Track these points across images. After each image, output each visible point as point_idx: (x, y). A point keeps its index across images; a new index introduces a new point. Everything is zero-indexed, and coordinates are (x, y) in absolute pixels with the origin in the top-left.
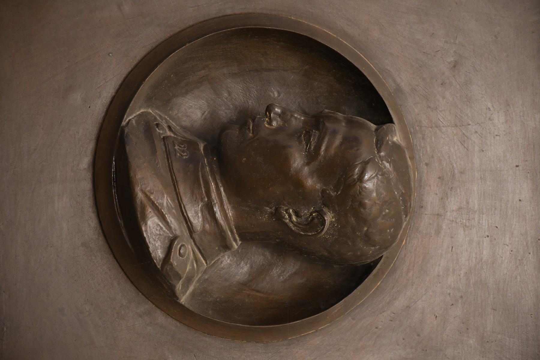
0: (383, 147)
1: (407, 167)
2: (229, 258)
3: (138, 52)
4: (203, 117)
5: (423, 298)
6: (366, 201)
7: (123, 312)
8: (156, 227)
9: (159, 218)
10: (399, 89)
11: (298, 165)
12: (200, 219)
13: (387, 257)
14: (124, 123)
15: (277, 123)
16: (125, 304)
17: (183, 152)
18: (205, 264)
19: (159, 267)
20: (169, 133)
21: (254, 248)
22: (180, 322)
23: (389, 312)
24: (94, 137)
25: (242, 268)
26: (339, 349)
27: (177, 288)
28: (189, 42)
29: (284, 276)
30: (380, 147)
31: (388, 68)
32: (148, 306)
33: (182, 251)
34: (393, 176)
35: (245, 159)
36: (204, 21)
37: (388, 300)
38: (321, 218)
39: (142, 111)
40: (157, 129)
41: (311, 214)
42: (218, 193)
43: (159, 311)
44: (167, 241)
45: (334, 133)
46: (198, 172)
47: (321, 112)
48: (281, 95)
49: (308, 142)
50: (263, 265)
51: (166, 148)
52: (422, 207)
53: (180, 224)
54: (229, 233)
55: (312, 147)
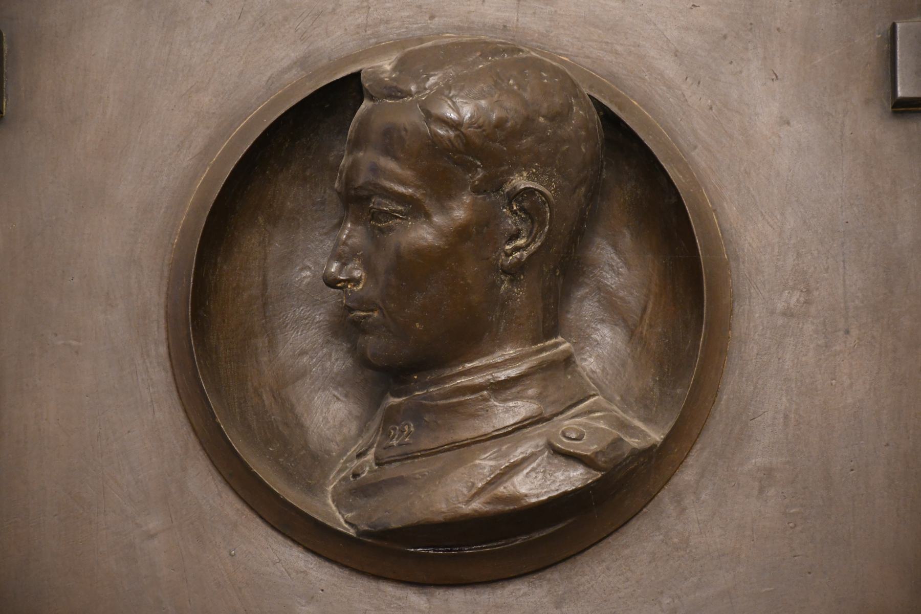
0: (402, 87)
1: (436, 47)
2: (585, 360)
3: (228, 505)
4: (344, 399)
5: (661, 27)
6: (494, 117)
7: (676, 540)
8: (531, 479)
9: (517, 473)
10: (302, 63)
11: (429, 233)
12: (520, 403)
13: (591, 87)
14: (352, 532)
15: (357, 269)
16: (661, 537)
17: (402, 431)
18: (597, 397)
19: (600, 475)
20: (370, 456)
21: (569, 316)
22: (694, 443)
23: (684, 87)
24: (372, 585)
25: (603, 337)
26: (746, 173)
27: (636, 445)
28: (214, 417)
29: (618, 266)
30: (401, 91)
31: (265, 79)
32: (665, 496)
33: (574, 436)
34: (451, 71)
35: (417, 325)
36: (178, 391)
37: (665, 88)
38: (522, 196)
39: (330, 501)
40: (363, 475)
41: (515, 212)
42: (477, 371)
43: (675, 480)
44: (556, 461)
45: (375, 169)
46: (437, 405)
47: (339, 193)
48: (309, 263)
49: (390, 215)
50: (599, 301)
51: (395, 461)
52: (505, 26)
53: (526, 438)
54: (544, 354)
55: (400, 208)
